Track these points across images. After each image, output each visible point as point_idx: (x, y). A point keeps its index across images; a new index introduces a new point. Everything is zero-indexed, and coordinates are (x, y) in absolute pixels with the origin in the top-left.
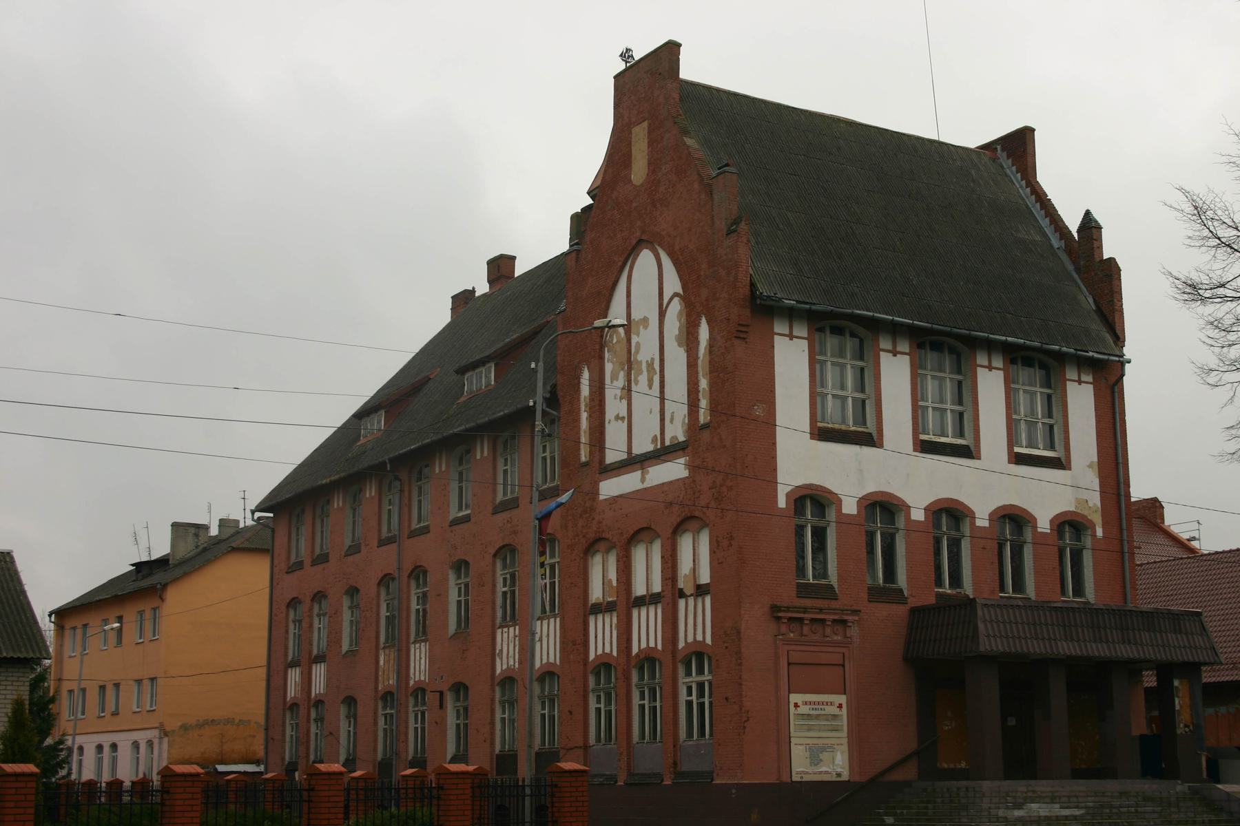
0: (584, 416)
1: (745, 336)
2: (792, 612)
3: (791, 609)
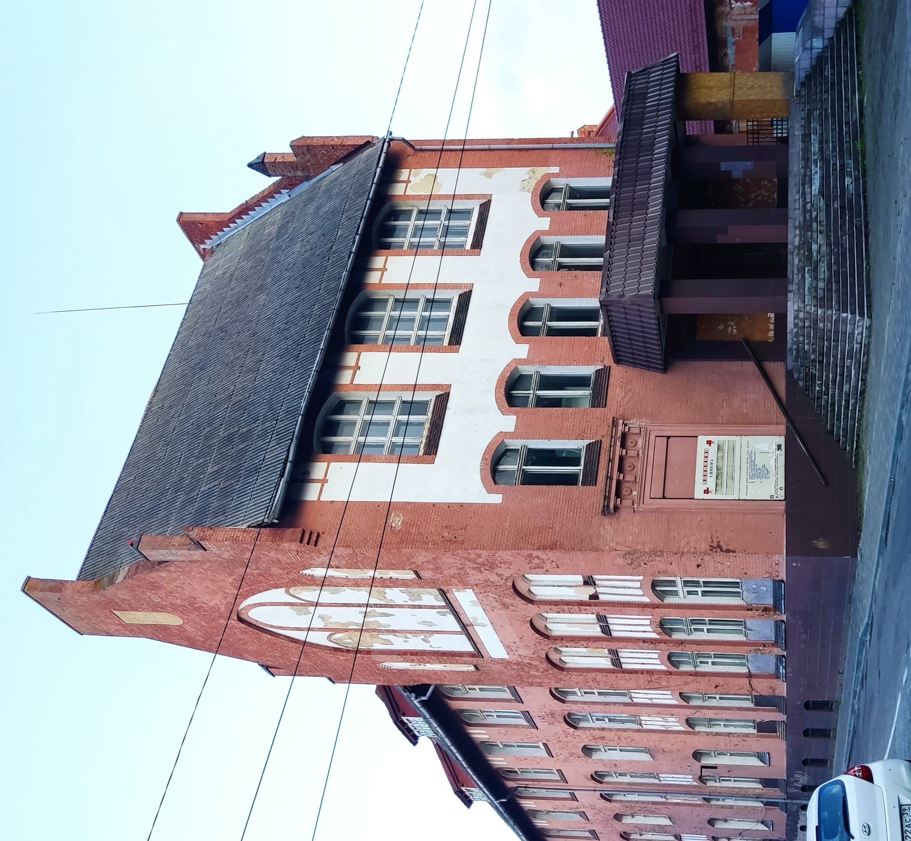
0: (429, 667)
1: (316, 534)
2: (610, 492)
3: (607, 495)
